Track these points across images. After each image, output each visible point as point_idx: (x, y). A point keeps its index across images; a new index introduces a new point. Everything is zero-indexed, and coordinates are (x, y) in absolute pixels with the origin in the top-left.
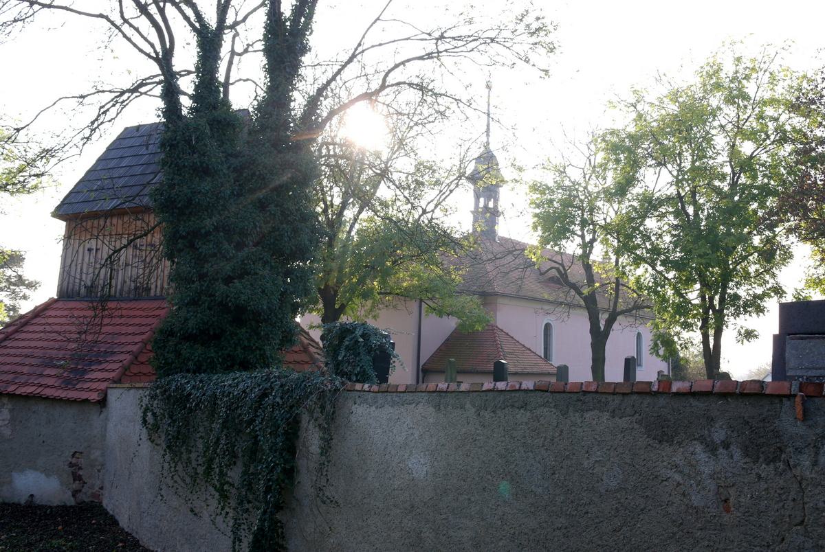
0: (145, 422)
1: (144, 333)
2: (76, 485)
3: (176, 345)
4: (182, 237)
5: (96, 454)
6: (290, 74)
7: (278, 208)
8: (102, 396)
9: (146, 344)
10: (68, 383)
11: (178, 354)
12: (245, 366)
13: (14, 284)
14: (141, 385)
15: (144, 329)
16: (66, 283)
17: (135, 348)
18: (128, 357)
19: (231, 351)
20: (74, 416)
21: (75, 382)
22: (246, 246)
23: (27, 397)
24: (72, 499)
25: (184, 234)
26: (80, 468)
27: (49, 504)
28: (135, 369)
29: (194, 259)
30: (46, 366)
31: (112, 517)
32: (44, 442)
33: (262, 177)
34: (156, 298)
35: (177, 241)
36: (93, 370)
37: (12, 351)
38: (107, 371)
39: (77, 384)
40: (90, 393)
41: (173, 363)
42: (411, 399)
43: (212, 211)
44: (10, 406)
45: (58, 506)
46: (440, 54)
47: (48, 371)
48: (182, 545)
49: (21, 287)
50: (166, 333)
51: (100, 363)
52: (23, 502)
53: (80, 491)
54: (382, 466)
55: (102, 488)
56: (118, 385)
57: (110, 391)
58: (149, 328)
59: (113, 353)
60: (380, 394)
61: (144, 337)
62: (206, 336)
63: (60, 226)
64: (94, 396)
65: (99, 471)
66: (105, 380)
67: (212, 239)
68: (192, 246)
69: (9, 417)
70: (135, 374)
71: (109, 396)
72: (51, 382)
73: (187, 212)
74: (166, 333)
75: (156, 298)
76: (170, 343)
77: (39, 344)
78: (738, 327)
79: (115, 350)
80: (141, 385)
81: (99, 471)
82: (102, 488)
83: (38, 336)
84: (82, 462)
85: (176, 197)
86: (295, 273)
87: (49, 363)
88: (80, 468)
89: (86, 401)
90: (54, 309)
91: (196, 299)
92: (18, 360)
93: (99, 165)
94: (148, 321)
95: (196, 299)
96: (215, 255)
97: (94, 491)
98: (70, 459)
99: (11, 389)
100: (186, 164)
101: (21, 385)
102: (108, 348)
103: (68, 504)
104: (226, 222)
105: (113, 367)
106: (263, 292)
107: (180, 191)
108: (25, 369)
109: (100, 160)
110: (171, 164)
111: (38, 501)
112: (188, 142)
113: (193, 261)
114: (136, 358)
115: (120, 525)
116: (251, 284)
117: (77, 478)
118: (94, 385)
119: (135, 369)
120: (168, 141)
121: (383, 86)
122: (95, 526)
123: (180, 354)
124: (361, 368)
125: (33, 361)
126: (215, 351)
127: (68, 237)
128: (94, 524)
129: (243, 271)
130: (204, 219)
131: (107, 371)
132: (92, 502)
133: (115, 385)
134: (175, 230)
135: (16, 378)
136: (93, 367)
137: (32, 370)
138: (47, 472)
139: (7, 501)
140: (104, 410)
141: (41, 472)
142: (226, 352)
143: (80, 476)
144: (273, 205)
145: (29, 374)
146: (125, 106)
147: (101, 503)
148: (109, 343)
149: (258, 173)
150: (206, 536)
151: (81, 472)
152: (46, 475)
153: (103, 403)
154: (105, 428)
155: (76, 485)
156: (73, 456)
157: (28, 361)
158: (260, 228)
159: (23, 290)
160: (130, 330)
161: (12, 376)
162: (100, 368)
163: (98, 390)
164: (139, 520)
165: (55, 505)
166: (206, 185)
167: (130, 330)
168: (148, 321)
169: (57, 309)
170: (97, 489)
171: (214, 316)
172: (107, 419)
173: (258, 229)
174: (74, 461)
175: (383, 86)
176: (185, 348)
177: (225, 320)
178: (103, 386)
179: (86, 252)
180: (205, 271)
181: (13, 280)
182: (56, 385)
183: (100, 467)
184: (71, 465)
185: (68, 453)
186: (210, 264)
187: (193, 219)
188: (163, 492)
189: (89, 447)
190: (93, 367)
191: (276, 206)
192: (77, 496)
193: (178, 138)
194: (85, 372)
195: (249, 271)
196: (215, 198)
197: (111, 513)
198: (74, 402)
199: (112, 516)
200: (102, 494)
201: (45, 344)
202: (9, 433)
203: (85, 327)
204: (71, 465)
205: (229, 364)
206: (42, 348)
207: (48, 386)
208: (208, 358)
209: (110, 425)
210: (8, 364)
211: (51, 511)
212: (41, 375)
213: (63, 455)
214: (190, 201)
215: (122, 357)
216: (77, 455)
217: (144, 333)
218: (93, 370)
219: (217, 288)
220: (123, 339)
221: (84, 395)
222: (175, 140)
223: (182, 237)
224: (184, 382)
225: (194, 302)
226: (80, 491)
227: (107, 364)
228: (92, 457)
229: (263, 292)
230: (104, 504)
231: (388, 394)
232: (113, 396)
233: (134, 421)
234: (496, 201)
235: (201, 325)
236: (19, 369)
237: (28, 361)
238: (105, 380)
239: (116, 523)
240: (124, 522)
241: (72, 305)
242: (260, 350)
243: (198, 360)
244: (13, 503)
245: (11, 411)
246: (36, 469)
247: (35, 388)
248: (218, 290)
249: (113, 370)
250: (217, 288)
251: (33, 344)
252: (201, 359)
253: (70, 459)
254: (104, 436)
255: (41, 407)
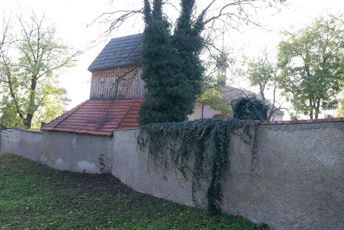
0: (138, 142)
1: (124, 111)
2: (102, 166)
3: (149, 112)
4: (153, 69)
5: (109, 155)
6: (191, 5)
7: (190, 58)
8: (112, 134)
9: (126, 115)
10: (98, 129)
11: (151, 116)
12: (177, 120)
13: (64, 100)
14: (124, 129)
15: (125, 110)
16: (93, 93)
17: (122, 117)
18: (120, 120)
19: (172, 115)
20: (100, 141)
21: (100, 129)
22: (177, 73)
23: (83, 134)
24: (100, 171)
25: (155, 67)
26: (103, 160)
27: (91, 173)
28: (122, 124)
29: (157, 77)
30: (89, 123)
31: (117, 179)
32: (89, 150)
33: (183, 45)
34: (127, 99)
35: (151, 70)
36: (106, 124)
37: (76, 118)
38: (112, 125)
39: (101, 129)
40: (107, 133)
41: (148, 119)
42: (319, 126)
43: (165, 58)
44: (76, 137)
45: (95, 174)
46: (240, 2)
47: (89, 125)
48: (156, 191)
49: (66, 101)
50: (144, 108)
51: (109, 122)
52: (81, 172)
53: (103, 169)
54: (295, 160)
55: (112, 168)
56: (117, 130)
57: (114, 132)
58: (126, 110)
59: (113, 118)
60: (291, 125)
61: (125, 113)
62: (162, 109)
63: (90, 74)
64: (108, 134)
65: (110, 161)
66: (112, 128)
67: (166, 69)
68: (157, 72)
69: (76, 141)
70: (123, 126)
71: (114, 134)
72: (91, 128)
73: (155, 58)
74: (144, 108)
75: (127, 99)
76: (147, 111)
77: (85, 115)
78: (325, 114)
79: (114, 117)
80: (124, 129)
81: (110, 161)
82: (112, 168)
83: (85, 112)
84: (104, 158)
85: (152, 51)
86: (195, 84)
87: (90, 122)
88: (103, 160)
89: (106, 135)
90: (89, 103)
91: (158, 93)
92: (78, 121)
93: (103, 52)
94: (125, 107)
95: (158, 93)
96: (166, 76)
97: (108, 169)
98: (99, 157)
99: (77, 131)
100: (156, 38)
101: (80, 130)
102: (111, 116)
103: (99, 173)
104: (171, 62)
105: (115, 124)
106: (186, 90)
107: (153, 49)
108: (81, 124)
109: (103, 50)
110: (149, 38)
111: (87, 172)
112: (156, 29)
113: (157, 78)
114: (123, 120)
115: (122, 181)
116: (182, 87)
117: (102, 164)
118: (108, 130)
119: (122, 124)
120: (148, 29)
121: (220, 15)
122: (112, 182)
123: (151, 115)
124: (256, 116)
125: (84, 121)
126: (166, 115)
127: (93, 79)
128: (111, 181)
129: (177, 82)
130: (162, 61)
131: (112, 125)
132: (108, 173)
133: (115, 130)
134: (150, 65)
135: (78, 127)
136: (106, 123)
137: (84, 124)
138: (91, 162)
139: (75, 172)
140: (112, 139)
141: (88, 162)
142: (170, 115)
143: (103, 163)
144: (188, 57)
145: (83, 126)
146: (123, 21)
147: (111, 173)
148: (111, 115)
149: (181, 43)
150: (169, 188)
151: (103, 162)
152: (90, 162)
153: (112, 136)
154: (112, 146)
155: (102, 166)
156: (100, 156)
157: (82, 121)
158: (183, 65)
159: (67, 102)
160: (119, 110)
161: (77, 126)
162: (109, 124)
163: (110, 132)
164: (132, 180)
165: (94, 173)
166: (164, 47)
167: (119, 110)
168: (125, 107)
169: (90, 103)
170: (110, 168)
171: (166, 101)
172: (113, 142)
173: (182, 66)
174: (101, 157)
175: (220, 15)
176: (154, 114)
177: (170, 102)
178: (112, 130)
179: (100, 83)
180: (162, 82)
181: (64, 99)
182: (93, 130)
183: (111, 160)
184: (100, 159)
185: (99, 155)
186: (164, 80)
187: (158, 61)
188: (149, 170)
189: (106, 152)
190: (106, 123)
191: (189, 57)
192: (102, 170)
193: (152, 28)
194: (104, 125)
195: (180, 82)
196: (167, 52)
197: (116, 177)
198: (99, 136)
199: (117, 178)
200: (112, 170)
201: (87, 115)
202: (76, 147)
203: (108, 107)
204: (100, 159)
205: (171, 120)
206: (86, 117)
207: (91, 130)
208: (163, 117)
209: (115, 145)
210: (84, 120)
211: (94, 176)
212: (87, 126)
213: (97, 155)
214: (157, 54)
215: (117, 120)
216: (102, 155)
217: (124, 111)
218: (106, 124)
219: (168, 89)
220: (116, 113)
221: (105, 133)
222: (151, 28)
223: (153, 69)
224: (154, 126)
225: (157, 95)
226: (103, 169)
227: (112, 122)
228: (108, 156)
229: (186, 90)
230: (113, 174)
231: (298, 124)
232: (117, 134)
233: (129, 143)
234: (225, 72)
235: (161, 104)
236: (79, 124)
237: (82, 121)
238: (112, 128)
239: (119, 181)
240: (123, 180)
241: (95, 102)
242: (183, 114)
243: (160, 118)
244: (78, 172)
245: (77, 139)
246: (87, 160)
247: (86, 131)
248: (168, 90)
249: (114, 125)
250: (168, 89)
251: (83, 115)
252: (161, 117)
253: (99, 157)
254: (112, 149)
255: (88, 138)
